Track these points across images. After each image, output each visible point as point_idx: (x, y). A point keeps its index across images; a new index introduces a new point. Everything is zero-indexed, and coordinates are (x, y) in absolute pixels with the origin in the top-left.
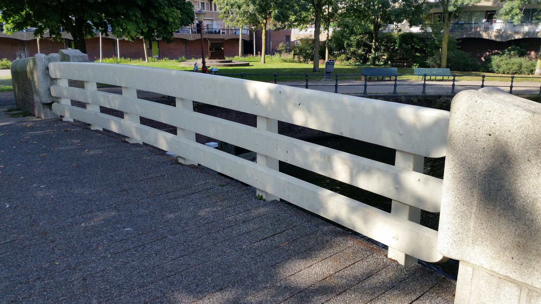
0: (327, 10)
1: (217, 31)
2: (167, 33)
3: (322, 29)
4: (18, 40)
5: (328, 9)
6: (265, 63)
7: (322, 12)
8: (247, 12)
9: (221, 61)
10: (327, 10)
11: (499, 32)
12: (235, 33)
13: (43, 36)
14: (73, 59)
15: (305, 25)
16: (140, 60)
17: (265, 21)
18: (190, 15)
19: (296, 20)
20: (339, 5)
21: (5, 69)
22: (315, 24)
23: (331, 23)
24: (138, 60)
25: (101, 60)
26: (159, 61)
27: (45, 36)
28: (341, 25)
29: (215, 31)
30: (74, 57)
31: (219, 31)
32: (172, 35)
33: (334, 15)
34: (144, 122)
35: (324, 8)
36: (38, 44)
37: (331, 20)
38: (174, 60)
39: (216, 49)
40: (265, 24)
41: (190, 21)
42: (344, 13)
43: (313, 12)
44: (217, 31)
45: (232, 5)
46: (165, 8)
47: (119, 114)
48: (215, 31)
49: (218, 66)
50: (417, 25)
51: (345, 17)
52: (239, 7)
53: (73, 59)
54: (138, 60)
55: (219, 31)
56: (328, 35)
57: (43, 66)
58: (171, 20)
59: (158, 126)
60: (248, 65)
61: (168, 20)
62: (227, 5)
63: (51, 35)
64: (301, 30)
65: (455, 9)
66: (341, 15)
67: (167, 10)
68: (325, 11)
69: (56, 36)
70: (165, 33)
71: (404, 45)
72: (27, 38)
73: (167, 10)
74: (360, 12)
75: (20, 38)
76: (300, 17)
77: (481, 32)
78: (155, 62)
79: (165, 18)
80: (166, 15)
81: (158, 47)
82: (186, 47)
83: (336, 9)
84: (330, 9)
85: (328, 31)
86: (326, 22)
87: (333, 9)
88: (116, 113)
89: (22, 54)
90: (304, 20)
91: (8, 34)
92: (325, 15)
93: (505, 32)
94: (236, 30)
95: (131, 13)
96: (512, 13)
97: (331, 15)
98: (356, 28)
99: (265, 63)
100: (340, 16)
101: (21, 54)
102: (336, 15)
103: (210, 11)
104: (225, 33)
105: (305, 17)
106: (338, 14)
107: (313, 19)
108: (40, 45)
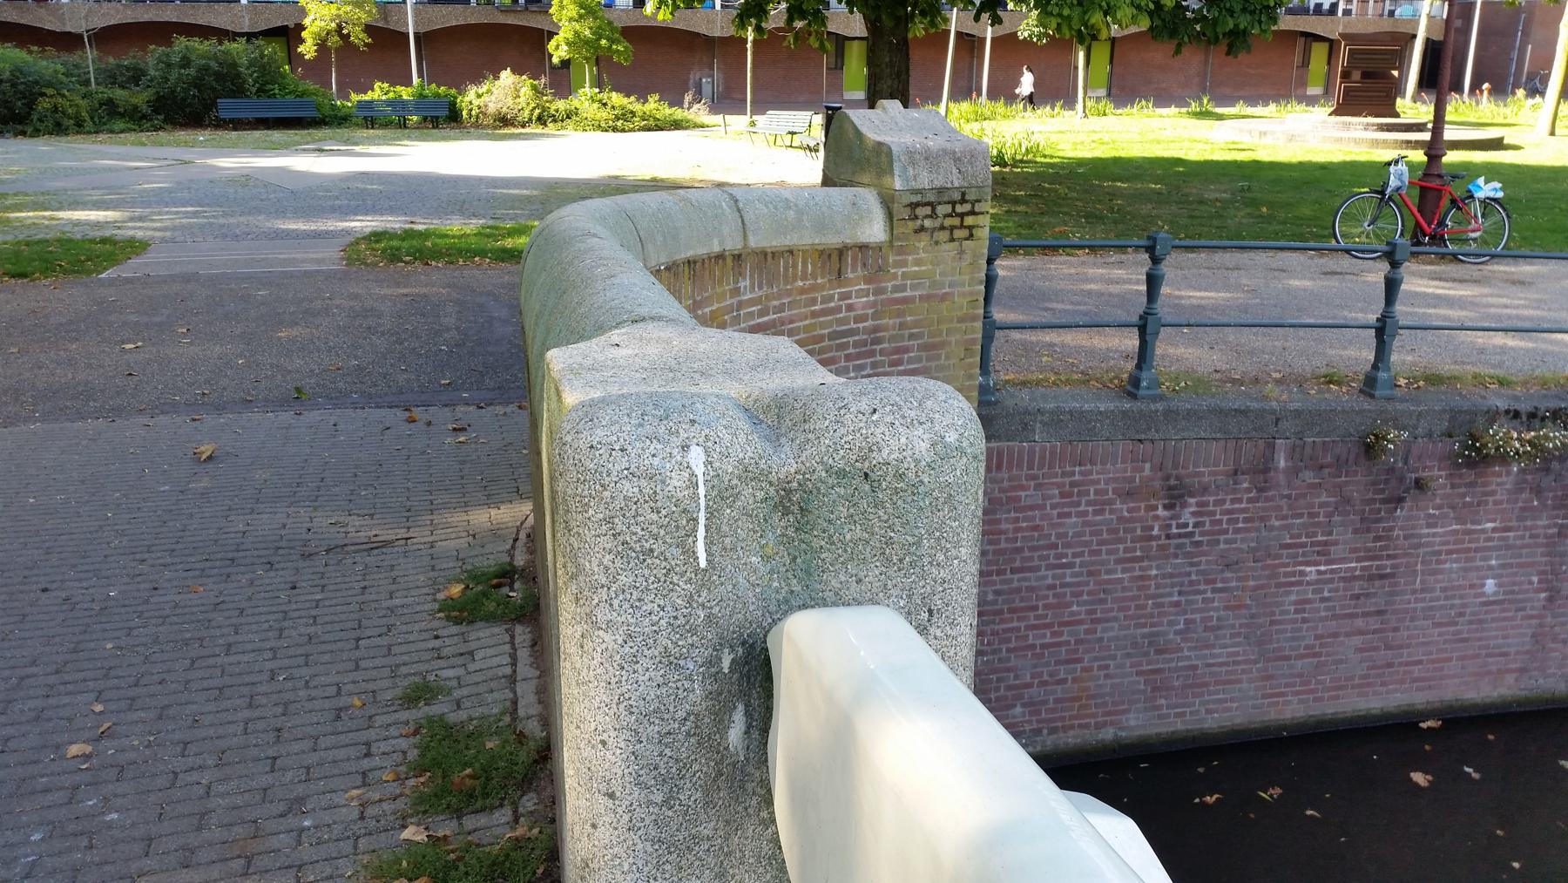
2: (1252, 13)
4: (698, 34)
6: (1552, 133)
9: (1387, 125)
13: (763, 25)
14: (911, 171)
16: (1057, 109)
21: (649, 129)
24: (1048, 108)
25: (942, 109)
26: (1119, 111)
27: (769, 25)
30: (913, 163)
32: (1274, 20)
34: (1220, 522)
36: (749, 53)
38: (1173, 110)
39: (1366, 75)
47: (1095, 477)
49: (1376, 143)
53: (911, 171)
54: (1048, 108)
57: (671, 662)
59: (1288, 546)
60: (1496, 144)
63: (790, 20)
69: (809, 24)
70: (1244, 10)
72: (722, 28)
75: (703, 30)
78: (1105, 115)
81: (1111, 62)
82: (1206, 62)
88: (1081, 473)
89: (704, 80)
91: (660, 17)
99: (1552, 133)
101: (701, 79)
104: (1354, 12)
108: (754, 54)
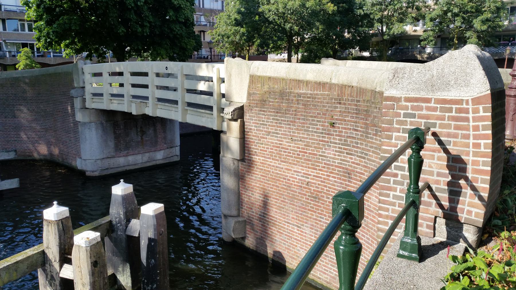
0: (296, 40)
1: (206, 57)
3: (293, 53)
5: (297, 39)
7: (293, 41)
8: (234, 41)
10: (296, 40)
11: (429, 55)
12: (221, 58)
15: (280, 51)
17: (248, 48)
18: (199, 44)
19: (273, 47)
20: (305, 36)
22: (288, 50)
23: (300, 50)
28: (308, 50)
29: (204, 57)
31: (208, 57)
33: (302, 43)
35: (294, 38)
37: (300, 47)
40: (248, 51)
41: (199, 48)
42: (310, 42)
43: (286, 41)
44: (206, 57)
45: (223, 36)
46: (185, 39)
48: (204, 57)
50: (365, 50)
51: (311, 44)
52: (228, 37)
55: (208, 57)
56: (298, 58)
58: (189, 47)
61: (187, 47)
62: (219, 36)
64: (277, 55)
65: (388, 37)
66: (307, 43)
67: (186, 40)
68: (295, 41)
71: (465, 152)
73: (186, 40)
74: (322, 41)
76: (277, 45)
77: (416, 55)
79: (185, 46)
80: (185, 43)
83: (303, 39)
84: (299, 39)
85: (298, 55)
86: (296, 49)
87: (301, 39)
90: (279, 47)
92: (295, 43)
93: (433, 54)
94: (221, 56)
95: (164, 42)
96: (428, 39)
97: (300, 44)
98: (319, 53)
100: (307, 44)
102: (303, 43)
103: (20, 32)
105: (280, 45)
106: (305, 43)
107: (286, 47)
